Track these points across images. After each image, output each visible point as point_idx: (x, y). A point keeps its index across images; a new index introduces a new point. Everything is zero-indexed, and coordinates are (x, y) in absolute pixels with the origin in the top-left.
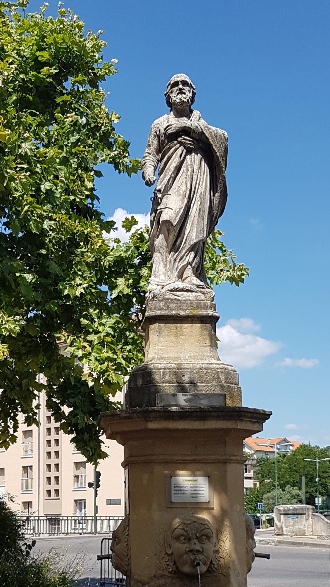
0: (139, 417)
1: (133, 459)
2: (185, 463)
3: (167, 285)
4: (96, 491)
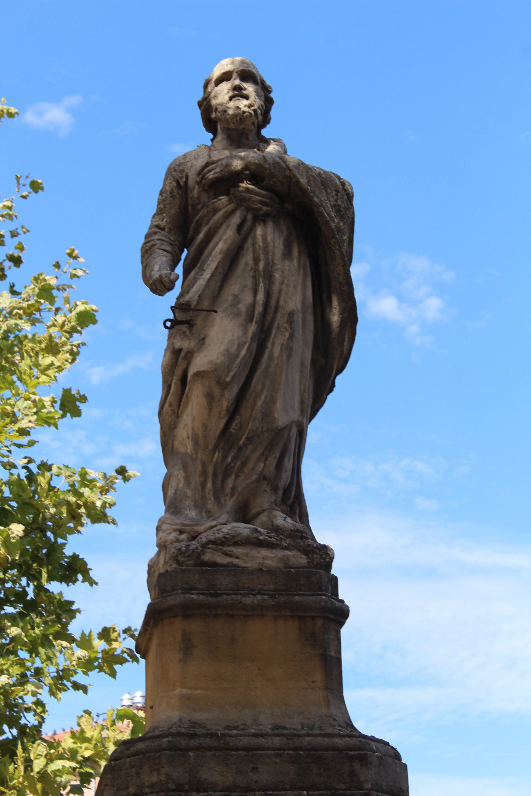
3: (205, 531)
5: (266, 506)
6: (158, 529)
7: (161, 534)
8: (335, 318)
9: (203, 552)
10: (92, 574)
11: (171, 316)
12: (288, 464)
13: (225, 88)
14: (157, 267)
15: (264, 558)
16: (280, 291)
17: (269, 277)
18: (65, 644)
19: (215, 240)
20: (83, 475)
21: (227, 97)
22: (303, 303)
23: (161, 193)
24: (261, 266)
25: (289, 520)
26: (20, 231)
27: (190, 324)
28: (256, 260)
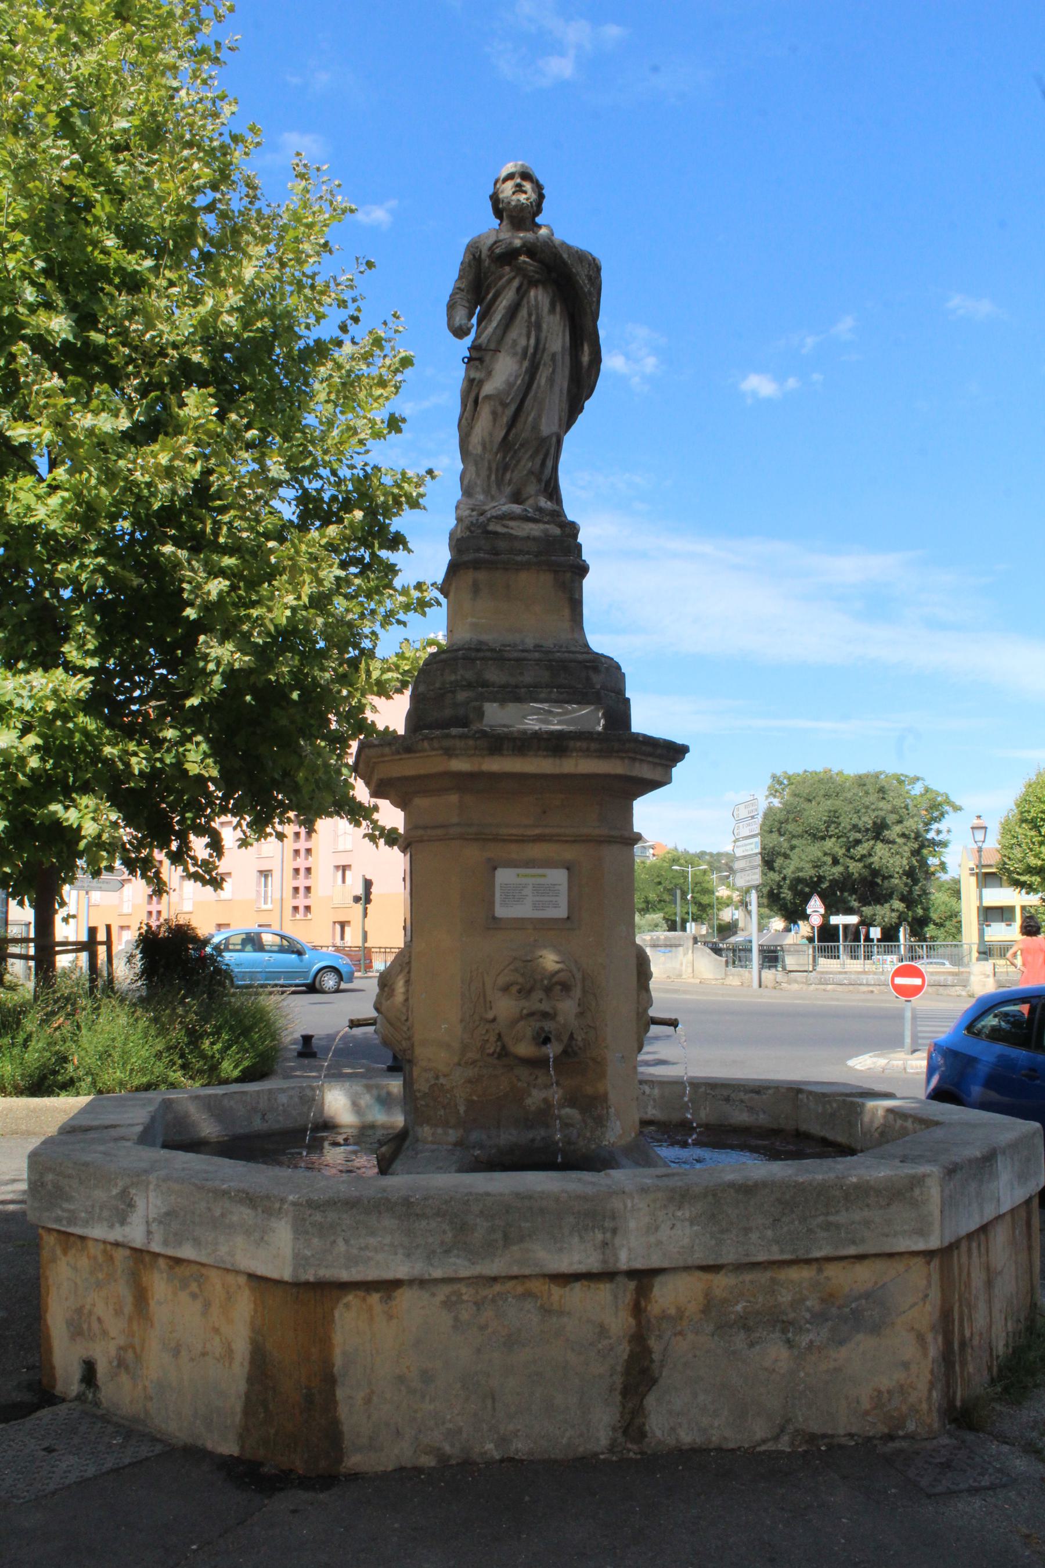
0: (433, 749)
1: (420, 832)
2: (523, 841)
4: (366, 909)
5: (533, 493)
6: (457, 508)
7: (459, 511)
8: (585, 359)
9: (488, 524)
10: (410, 545)
11: (468, 354)
12: (549, 464)
13: (510, 184)
14: (458, 319)
15: (531, 529)
16: (546, 338)
17: (538, 327)
18: (391, 592)
19: (500, 299)
20: (404, 474)
21: (511, 192)
22: (563, 347)
23: (462, 263)
24: (533, 318)
25: (549, 503)
26: (359, 298)
27: (481, 360)
28: (530, 315)
